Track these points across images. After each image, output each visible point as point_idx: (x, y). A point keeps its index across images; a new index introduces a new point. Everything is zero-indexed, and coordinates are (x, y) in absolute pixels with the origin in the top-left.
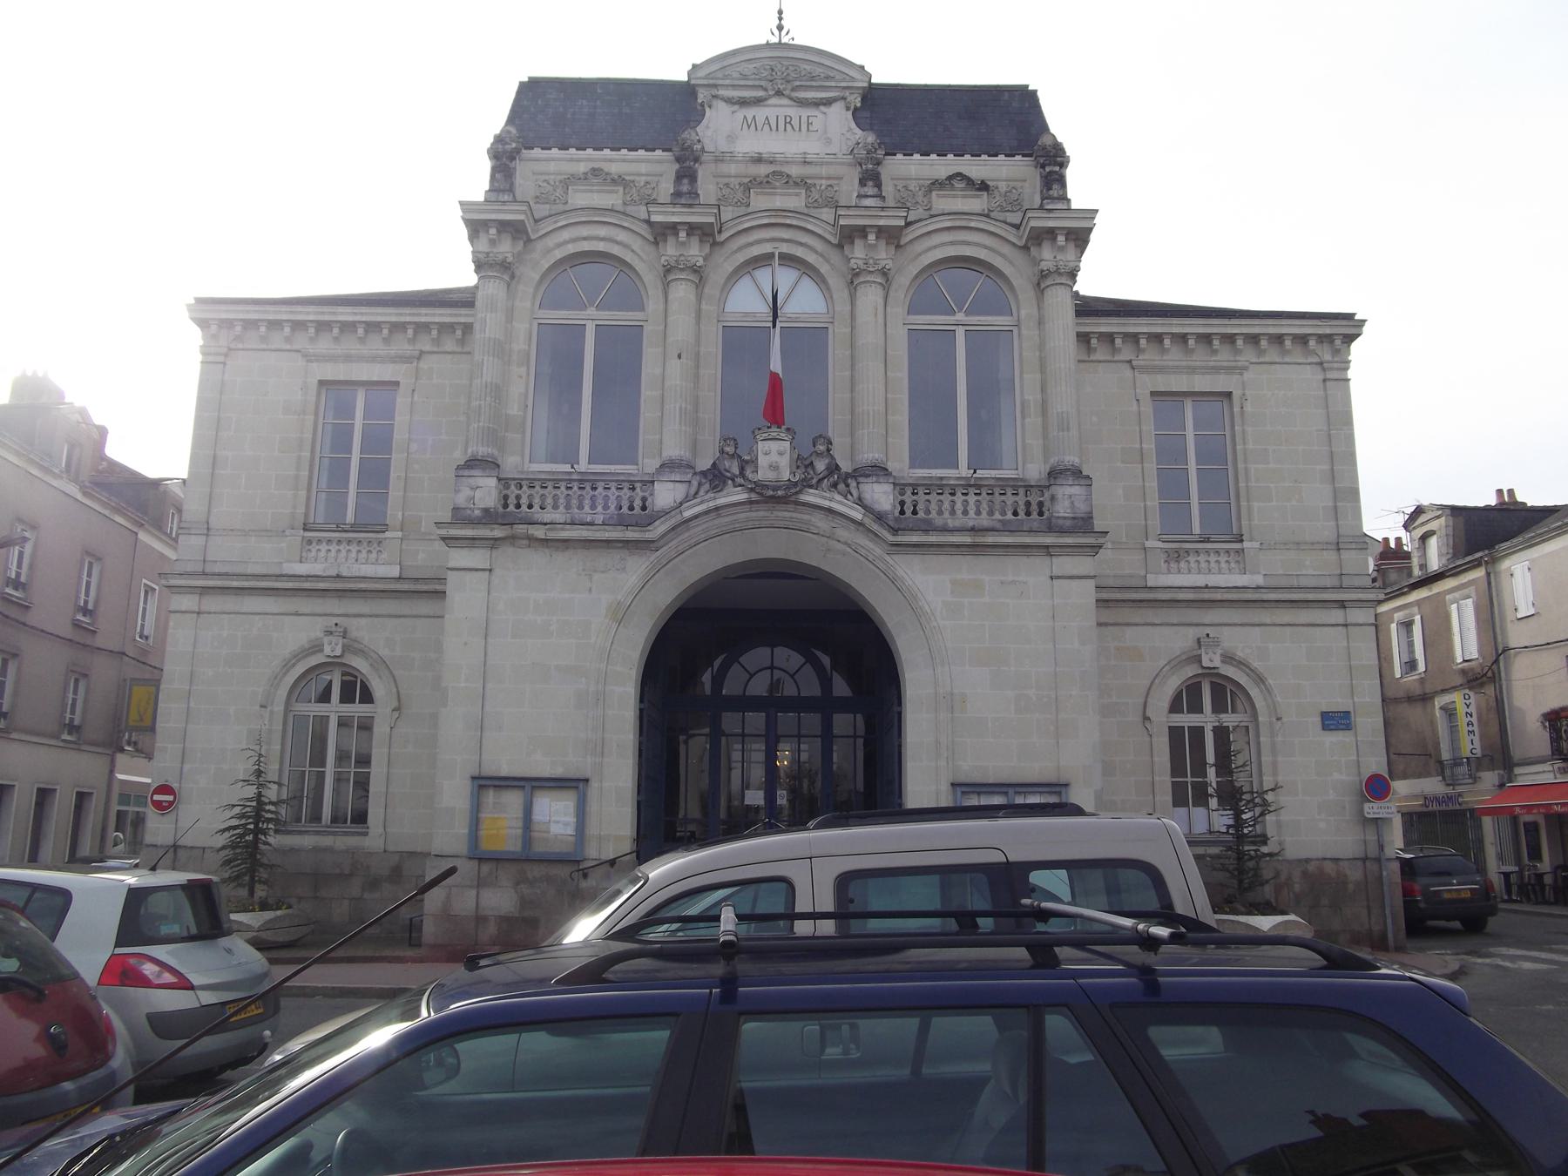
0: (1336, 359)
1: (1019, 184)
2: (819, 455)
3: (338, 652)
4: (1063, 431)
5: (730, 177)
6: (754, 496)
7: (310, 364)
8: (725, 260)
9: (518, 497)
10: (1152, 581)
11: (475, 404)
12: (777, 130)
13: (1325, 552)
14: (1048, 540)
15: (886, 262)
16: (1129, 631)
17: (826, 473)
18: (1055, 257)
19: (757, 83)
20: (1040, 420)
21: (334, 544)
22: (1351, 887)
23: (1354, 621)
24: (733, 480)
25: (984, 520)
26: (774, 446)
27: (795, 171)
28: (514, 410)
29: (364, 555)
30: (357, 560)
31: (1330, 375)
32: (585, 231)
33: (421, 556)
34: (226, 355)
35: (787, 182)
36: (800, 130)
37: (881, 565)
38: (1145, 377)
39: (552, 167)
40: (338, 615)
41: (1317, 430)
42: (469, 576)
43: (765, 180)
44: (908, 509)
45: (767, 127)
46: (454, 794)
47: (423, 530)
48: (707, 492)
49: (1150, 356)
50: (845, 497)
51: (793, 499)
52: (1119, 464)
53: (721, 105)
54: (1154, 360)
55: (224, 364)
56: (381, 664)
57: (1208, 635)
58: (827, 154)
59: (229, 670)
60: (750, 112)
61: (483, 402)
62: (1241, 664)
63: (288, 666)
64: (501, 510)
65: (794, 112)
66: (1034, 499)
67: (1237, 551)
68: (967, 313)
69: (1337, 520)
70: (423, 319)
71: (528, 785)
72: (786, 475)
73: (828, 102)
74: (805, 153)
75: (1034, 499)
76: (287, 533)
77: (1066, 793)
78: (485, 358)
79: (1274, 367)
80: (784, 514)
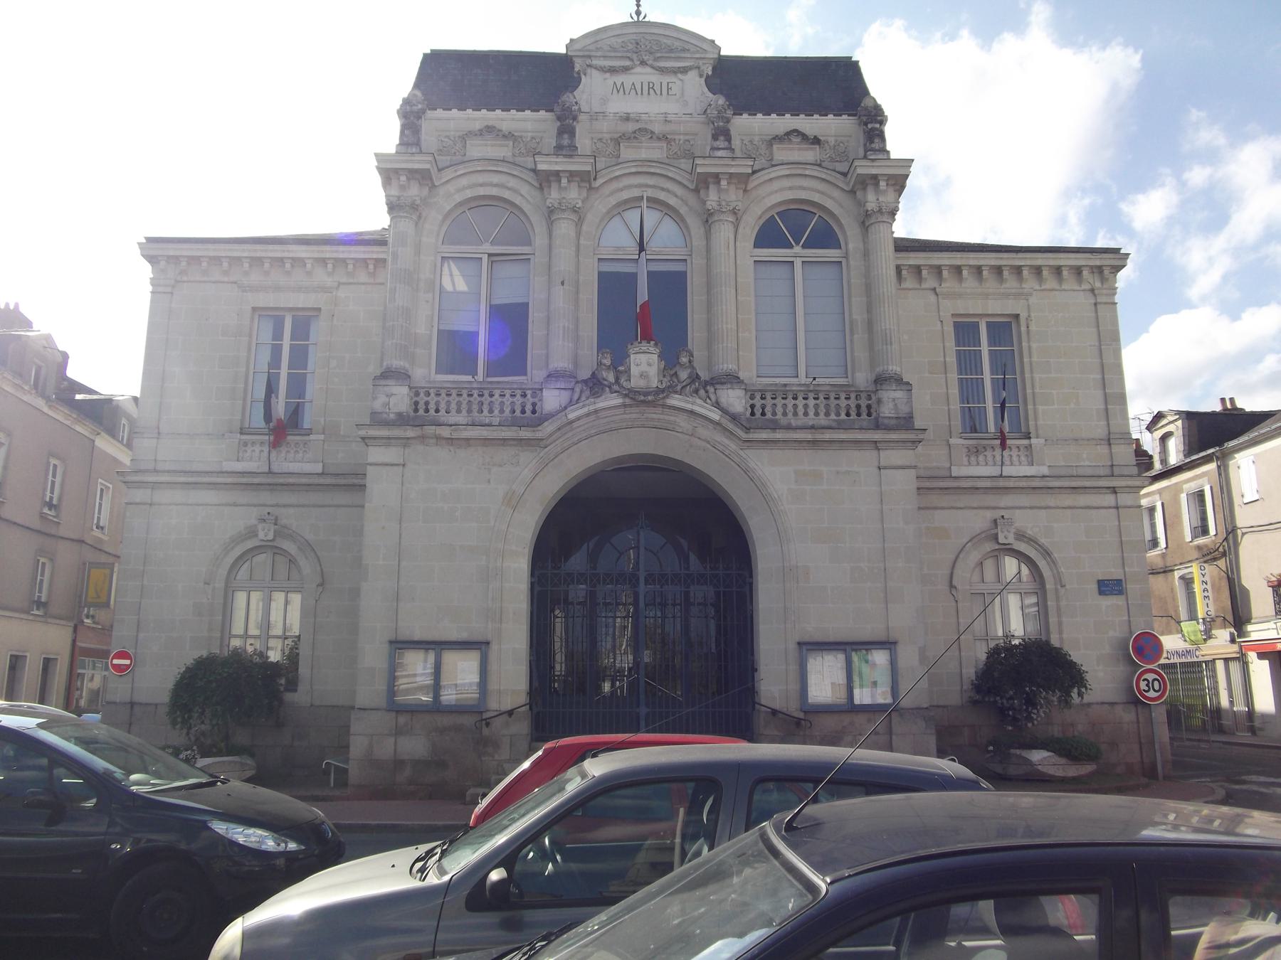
9: (427, 403)
12: (642, 94)
17: (688, 381)
18: (878, 200)
19: (625, 54)
24: (610, 387)
25: (822, 420)
27: (657, 128)
32: (480, 179)
34: (173, 287)
36: (661, 94)
37: (736, 459)
41: (1091, 346)
45: (633, 91)
46: (373, 655)
47: (342, 433)
48: (588, 398)
50: (705, 401)
52: (927, 375)
53: (595, 73)
57: (1003, 517)
60: (619, 79)
62: (1032, 541)
65: (655, 78)
68: (804, 247)
70: (341, 256)
72: (654, 383)
73: (684, 70)
74: (666, 113)
75: (864, 403)
80: (654, 414)
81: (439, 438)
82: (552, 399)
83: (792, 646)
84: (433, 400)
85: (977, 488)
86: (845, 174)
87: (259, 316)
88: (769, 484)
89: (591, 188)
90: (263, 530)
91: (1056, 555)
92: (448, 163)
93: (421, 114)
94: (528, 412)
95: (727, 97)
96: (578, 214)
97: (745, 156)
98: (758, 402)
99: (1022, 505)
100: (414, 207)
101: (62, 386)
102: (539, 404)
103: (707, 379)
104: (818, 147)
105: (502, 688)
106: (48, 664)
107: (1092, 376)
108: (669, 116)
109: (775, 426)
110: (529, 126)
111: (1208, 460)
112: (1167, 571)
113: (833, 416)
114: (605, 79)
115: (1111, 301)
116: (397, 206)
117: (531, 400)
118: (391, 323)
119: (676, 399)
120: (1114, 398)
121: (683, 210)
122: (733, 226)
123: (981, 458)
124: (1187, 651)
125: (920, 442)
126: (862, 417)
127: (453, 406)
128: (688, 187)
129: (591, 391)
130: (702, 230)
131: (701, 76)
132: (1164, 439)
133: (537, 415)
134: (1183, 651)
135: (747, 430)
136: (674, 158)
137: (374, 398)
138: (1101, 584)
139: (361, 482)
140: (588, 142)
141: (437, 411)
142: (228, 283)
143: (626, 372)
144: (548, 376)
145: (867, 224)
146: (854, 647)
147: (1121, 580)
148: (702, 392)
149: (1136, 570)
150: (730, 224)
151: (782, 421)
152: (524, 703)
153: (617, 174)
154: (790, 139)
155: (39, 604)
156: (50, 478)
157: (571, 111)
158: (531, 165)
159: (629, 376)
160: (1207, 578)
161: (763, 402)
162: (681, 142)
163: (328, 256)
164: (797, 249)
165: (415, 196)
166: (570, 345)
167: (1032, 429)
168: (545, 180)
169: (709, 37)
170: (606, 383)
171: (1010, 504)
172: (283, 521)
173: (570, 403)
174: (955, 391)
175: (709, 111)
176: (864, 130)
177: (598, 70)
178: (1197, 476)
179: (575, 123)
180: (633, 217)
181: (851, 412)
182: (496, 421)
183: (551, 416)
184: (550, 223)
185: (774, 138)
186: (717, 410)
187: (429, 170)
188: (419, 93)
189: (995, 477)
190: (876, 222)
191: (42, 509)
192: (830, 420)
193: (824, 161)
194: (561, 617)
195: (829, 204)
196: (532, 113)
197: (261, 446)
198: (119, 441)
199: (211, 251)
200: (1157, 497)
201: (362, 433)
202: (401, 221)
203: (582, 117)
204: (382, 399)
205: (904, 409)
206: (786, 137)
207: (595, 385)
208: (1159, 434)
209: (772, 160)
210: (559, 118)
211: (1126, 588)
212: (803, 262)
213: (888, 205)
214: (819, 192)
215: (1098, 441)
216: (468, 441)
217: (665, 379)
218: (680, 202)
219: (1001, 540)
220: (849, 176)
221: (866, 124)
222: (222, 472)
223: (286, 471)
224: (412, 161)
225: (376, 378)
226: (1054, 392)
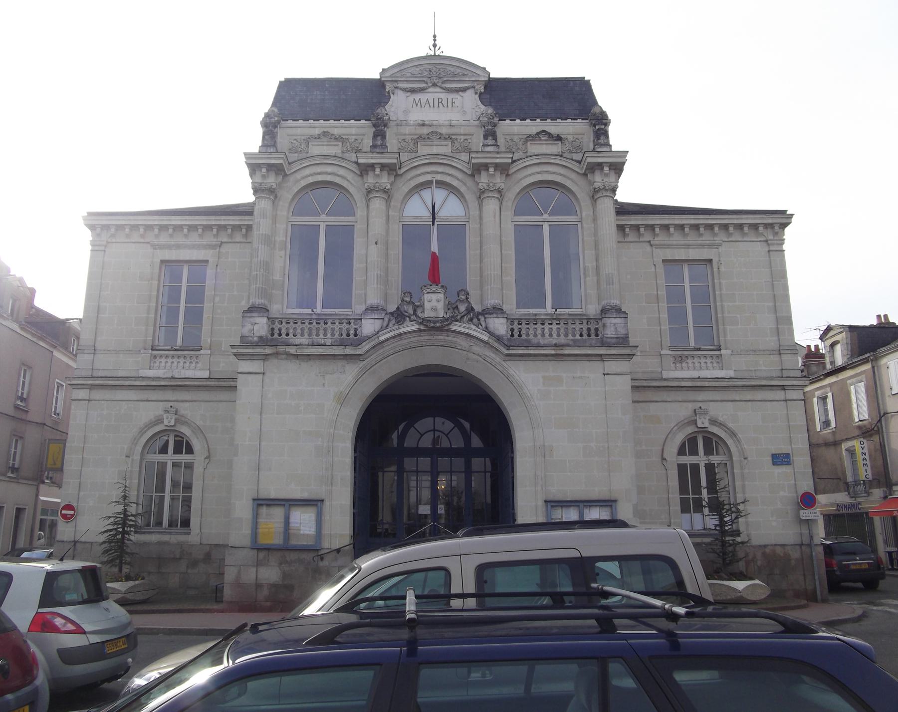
1: (580, 137)
2: (462, 301)
6: (422, 327)
9: (280, 329)
12: (434, 106)
13: (772, 356)
16: (652, 406)
17: (465, 312)
18: (603, 180)
19: (421, 79)
20: (595, 278)
22: (793, 562)
24: (409, 317)
25: (562, 340)
27: (444, 131)
28: (277, 277)
31: (772, 248)
32: (319, 169)
33: (222, 365)
34: (106, 246)
36: (447, 106)
39: (299, 131)
41: (765, 282)
42: (250, 377)
45: (427, 105)
46: (243, 509)
48: (394, 325)
49: (661, 238)
50: (478, 327)
51: (446, 328)
52: (644, 304)
53: (400, 93)
55: (105, 251)
56: (198, 430)
57: (700, 407)
60: (417, 97)
62: (721, 425)
63: (142, 432)
65: (444, 96)
68: (550, 214)
72: (441, 314)
73: (464, 90)
75: (593, 327)
77: (615, 506)
78: (260, 246)
79: (737, 243)
80: (440, 337)
82: (369, 326)
83: (541, 503)
84: (284, 326)
85: (682, 387)
86: (579, 162)
87: (165, 265)
88: (523, 385)
89: (397, 176)
90: (167, 418)
91: (740, 436)
92: (296, 159)
93: (277, 124)
94: (352, 336)
95: (495, 108)
96: (387, 194)
97: (508, 150)
98: (516, 327)
99: (715, 399)
100: (271, 191)
101: (31, 313)
102: (359, 330)
103: (480, 311)
104: (560, 142)
105: (332, 533)
106: (19, 511)
108: (453, 122)
109: (528, 344)
110: (353, 131)
111: (865, 361)
112: (836, 444)
113: (570, 337)
114: (407, 97)
115: (780, 249)
116: (260, 189)
117: (354, 327)
118: (255, 273)
120: (784, 321)
121: (463, 189)
122: (498, 201)
123: (684, 364)
124: (852, 505)
125: (634, 355)
126: (591, 337)
127: (299, 331)
128: (466, 173)
129: (396, 320)
130: (477, 203)
131: (476, 93)
132: (833, 345)
133: (357, 337)
134: (849, 505)
135: (508, 347)
136: (457, 153)
137: (243, 326)
139: (232, 384)
140: (395, 141)
141: (287, 335)
142: (143, 243)
143: (421, 306)
144: (366, 310)
145: (595, 198)
146: (585, 504)
147: (789, 454)
148: (475, 320)
149: (800, 446)
150: (496, 199)
151: (533, 340)
152: (348, 544)
153: (416, 164)
154: (540, 138)
155: (14, 469)
156: (22, 379)
157: (383, 120)
158: (354, 159)
159: (424, 309)
160: (866, 450)
161: (520, 326)
162: (462, 140)
163: (213, 223)
165: (273, 183)
166: (382, 287)
167: (722, 344)
168: (365, 169)
169: (482, 66)
170: (406, 314)
171: (705, 398)
173: (382, 329)
174: (665, 316)
175: (481, 119)
176: (593, 129)
177: (402, 90)
178: (857, 374)
179: (385, 129)
180: (426, 194)
181: (583, 333)
182: (329, 342)
183: (368, 338)
184: (368, 201)
185: (528, 137)
186: (486, 333)
187: (282, 164)
188: (276, 110)
189: (695, 378)
190: (601, 197)
191: (15, 402)
192: (568, 339)
193: (565, 153)
196: (356, 122)
198: (70, 352)
199: (133, 221)
200: (828, 389)
201: (235, 351)
202: (262, 200)
203: (391, 124)
204: (249, 327)
205: (622, 331)
207: (399, 316)
208: (829, 342)
209: (526, 152)
210: (374, 126)
211: (793, 460)
213: (610, 184)
214: (560, 174)
215: (771, 352)
216: (309, 357)
217: (449, 311)
218: (461, 184)
219: (700, 425)
220: (582, 163)
221: (594, 126)
222: (139, 378)
223: (183, 376)
224: (270, 158)
225: (244, 312)
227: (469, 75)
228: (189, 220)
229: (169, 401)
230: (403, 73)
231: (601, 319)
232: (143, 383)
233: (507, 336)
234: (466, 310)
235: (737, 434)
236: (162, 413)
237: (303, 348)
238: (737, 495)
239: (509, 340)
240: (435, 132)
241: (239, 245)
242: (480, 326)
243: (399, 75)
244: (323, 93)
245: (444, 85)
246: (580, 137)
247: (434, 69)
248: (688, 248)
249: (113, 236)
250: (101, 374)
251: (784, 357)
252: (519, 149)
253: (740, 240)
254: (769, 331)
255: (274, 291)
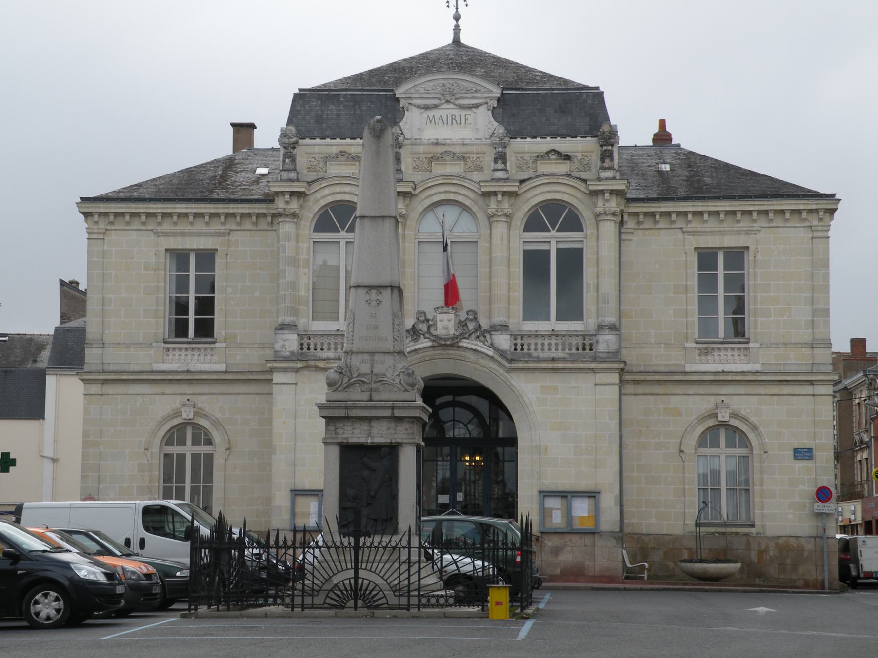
0: (820, 224)
1: (588, 154)
2: (471, 320)
3: (191, 416)
4: (605, 303)
5: (420, 153)
6: (435, 344)
7: (159, 238)
8: (418, 205)
9: (309, 345)
10: (688, 368)
11: (282, 293)
12: (447, 124)
13: (803, 349)
14: (593, 365)
15: (508, 210)
16: (673, 398)
17: (473, 331)
18: (604, 205)
19: (435, 95)
20: (595, 294)
21: (183, 351)
22: (806, 554)
23: (818, 393)
24: (424, 335)
25: (560, 354)
26: (445, 316)
27: (457, 149)
28: (302, 293)
29: (196, 357)
30: (198, 360)
31: (816, 234)
32: (337, 189)
33: (238, 357)
34: (104, 234)
35: (453, 158)
36: (461, 124)
37: (503, 378)
38: (692, 238)
39: (317, 149)
40: (189, 394)
41: (805, 271)
42: (284, 387)
43: (441, 156)
44: (519, 347)
45: (441, 121)
46: (281, 499)
47: (238, 341)
48: (410, 342)
50: (484, 343)
51: (456, 345)
52: (672, 295)
53: (415, 110)
54: (697, 227)
55: (104, 239)
56: (216, 423)
57: (723, 401)
58: (476, 139)
59: (123, 429)
60: (431, 113)
61: (287, 293)
62: (744, 419)
63: (160, 425)
64: (300, 351)
65: (457, 112)
66: (587, 342)
67: (746, 349)
68: (558, 231)
69: (813, 329)
70: (231, 211)
71: (569, 495)
72: (452, 332)
73: (477, 106)
74: (463, 139)
75: (587, 342)
76: (154, 344)
77: (599, 496)
78: (287, 268)
79: (778, 229)
80: (452, 352)
81: (317, 367)
83: (535, 493)
84: (312, 342)
92: (315, 178)
107: (804, 295)
118: (284, 293)
119: (466, 342)
123: (709, 357)
131: (489, 110)
138: (796, 451)
146: (573, 494)
153: (430, 184)
163: (221, 211)
164: (553, 233)
172: (200, 405)
185: (538, 157)
194: (304, 553)
195: (574, 202)
197: (179, 351)
206: (546, 156)
212: (557, 241)
217: (459, 329)
218: (473, 203)
226: (772, 307)
227: (483, 90)
228: (195, 208)
229: (185, 394)
230: (417, 89)
231: (595, 335)
232: (159, 377)
233: (510, 351)
234: (474, 328)
235: (758, 428)
236: (180, 406)
237: (330, 363)
238: (755, 488)
239: (512, 354)
240: (448, 151)
241: (248, 232)
242: (486, 343)
243: (413, 91)
244: (338, 108)
245: (457, 102)
246: (588, 154)
247: (447, 84)
248: (724, 235)
249: (112, 223)
250: (112, 368)
251: (816, 351)
252: (529, 167)
253: (781, 225)
254: (803, 324)
255: (301, 307)
